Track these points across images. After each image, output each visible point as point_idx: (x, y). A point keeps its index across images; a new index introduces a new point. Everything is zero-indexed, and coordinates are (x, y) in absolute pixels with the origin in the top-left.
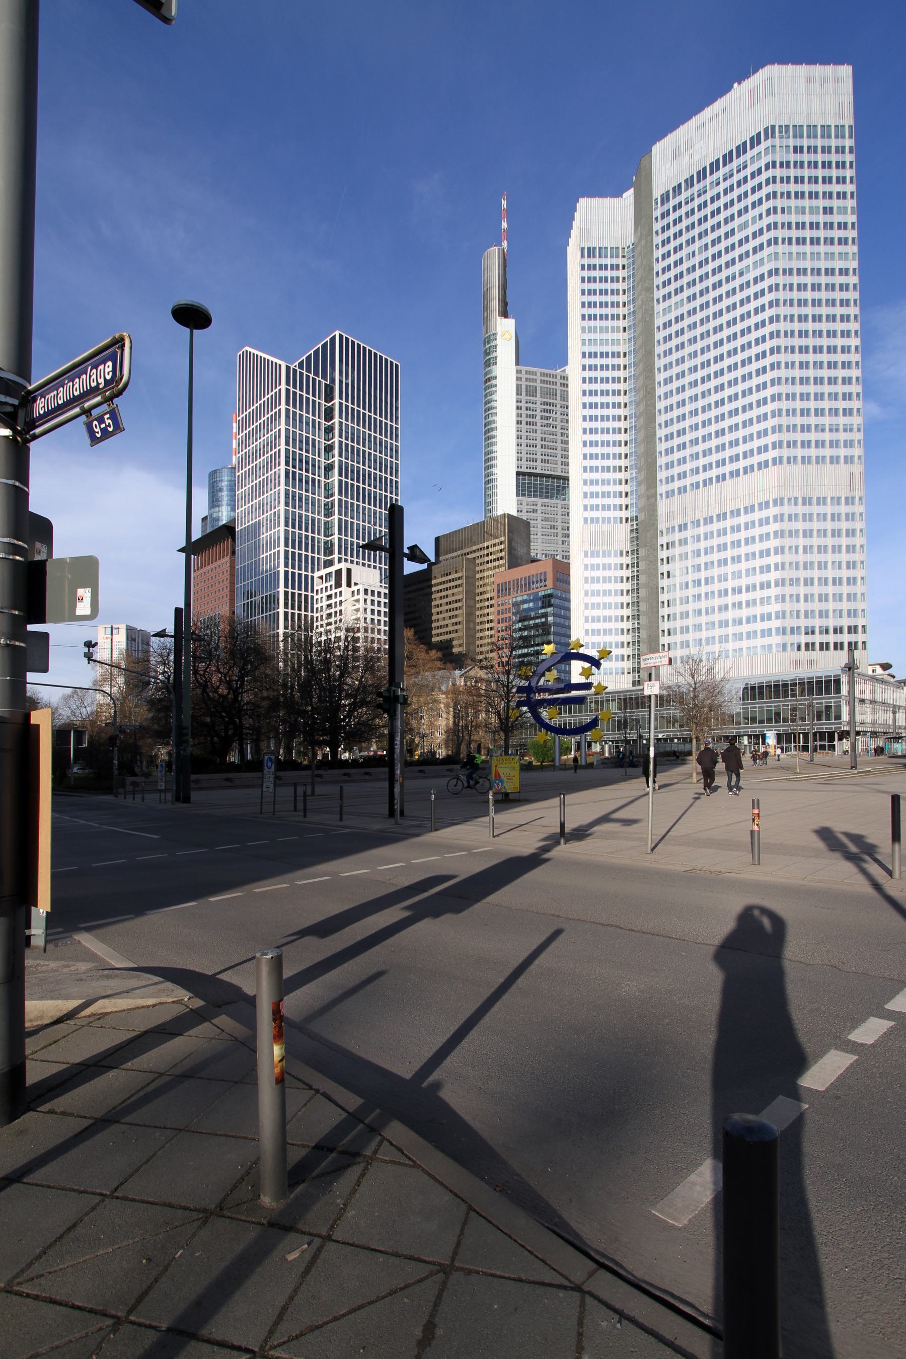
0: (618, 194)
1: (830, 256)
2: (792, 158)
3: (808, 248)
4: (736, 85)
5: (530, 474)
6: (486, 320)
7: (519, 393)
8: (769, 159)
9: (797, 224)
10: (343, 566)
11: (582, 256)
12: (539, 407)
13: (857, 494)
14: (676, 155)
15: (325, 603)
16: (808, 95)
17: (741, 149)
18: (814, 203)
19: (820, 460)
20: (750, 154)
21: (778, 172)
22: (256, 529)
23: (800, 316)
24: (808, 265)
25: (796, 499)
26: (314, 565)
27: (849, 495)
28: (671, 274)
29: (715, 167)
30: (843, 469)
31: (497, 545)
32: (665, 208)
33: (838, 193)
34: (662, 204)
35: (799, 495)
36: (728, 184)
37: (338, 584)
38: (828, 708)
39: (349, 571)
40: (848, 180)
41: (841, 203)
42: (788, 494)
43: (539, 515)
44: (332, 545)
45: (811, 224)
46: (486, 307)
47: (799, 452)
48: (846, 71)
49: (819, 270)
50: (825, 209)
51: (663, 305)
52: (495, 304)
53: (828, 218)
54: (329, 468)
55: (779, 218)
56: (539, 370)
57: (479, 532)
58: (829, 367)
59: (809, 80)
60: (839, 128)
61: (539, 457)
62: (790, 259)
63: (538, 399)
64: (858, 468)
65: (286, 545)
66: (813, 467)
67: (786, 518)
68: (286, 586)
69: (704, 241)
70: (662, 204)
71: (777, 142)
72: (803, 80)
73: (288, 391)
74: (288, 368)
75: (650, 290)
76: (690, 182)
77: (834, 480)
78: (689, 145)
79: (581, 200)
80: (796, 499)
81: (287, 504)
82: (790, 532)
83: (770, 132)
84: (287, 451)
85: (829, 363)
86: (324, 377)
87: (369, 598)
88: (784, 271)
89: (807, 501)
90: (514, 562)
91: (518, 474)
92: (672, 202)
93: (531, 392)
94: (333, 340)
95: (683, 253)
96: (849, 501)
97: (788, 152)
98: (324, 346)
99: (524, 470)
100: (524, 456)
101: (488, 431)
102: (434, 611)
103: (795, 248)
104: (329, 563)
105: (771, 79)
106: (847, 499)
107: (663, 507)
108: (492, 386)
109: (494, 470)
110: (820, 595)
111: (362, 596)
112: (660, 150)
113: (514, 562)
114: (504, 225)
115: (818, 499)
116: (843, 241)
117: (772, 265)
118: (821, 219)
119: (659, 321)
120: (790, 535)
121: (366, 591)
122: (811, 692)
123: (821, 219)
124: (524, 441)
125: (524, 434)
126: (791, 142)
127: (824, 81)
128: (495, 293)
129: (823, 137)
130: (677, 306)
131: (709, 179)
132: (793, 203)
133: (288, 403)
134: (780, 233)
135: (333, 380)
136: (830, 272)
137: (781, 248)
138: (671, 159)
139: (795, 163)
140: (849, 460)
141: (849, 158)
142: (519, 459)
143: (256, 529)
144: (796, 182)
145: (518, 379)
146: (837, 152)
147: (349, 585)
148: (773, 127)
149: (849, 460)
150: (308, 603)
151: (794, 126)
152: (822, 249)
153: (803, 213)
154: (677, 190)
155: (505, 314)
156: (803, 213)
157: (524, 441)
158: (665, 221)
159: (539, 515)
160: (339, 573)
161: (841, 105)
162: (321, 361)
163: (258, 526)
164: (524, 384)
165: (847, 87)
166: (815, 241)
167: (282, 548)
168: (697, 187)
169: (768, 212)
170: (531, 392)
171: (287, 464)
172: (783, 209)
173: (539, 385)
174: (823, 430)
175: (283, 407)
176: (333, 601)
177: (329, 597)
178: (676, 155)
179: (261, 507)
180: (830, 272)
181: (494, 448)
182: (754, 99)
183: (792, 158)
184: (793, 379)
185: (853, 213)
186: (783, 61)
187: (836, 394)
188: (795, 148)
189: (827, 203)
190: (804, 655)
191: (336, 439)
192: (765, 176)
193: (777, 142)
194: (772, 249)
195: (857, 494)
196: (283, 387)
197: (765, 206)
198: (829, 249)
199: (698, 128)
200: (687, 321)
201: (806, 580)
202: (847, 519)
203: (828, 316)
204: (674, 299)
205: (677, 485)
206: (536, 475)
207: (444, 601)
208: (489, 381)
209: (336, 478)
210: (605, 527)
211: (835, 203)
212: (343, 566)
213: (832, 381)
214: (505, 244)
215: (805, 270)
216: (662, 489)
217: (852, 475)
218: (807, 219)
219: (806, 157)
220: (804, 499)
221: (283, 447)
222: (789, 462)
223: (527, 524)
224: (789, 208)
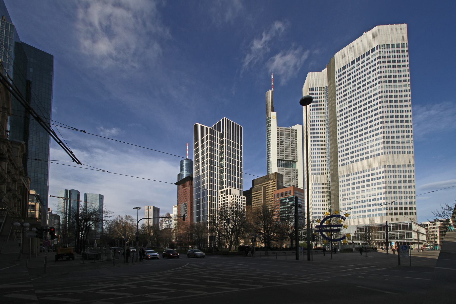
0: (321, 70)
1: (401, 86)
2: (386, 55)
3: (393, 84)
4: (364, 33)
5: (282, 160)
6: (267, 113)
7: (278, 135)
8: (378, 55)
9: (389, 76)
10: (228, 188)
11: (310, 91)
12: (284, 139)
13: (412, 164)
14: (343, 56)
15: (222, 200)
16: (394, 34)
17: (368, 53)
18: (395, 69)
19: (398, 153)
20: (371, 54)
21: (382, 60)
22: (200, 177)
23: (390, 106)
24: (393, 89)
25: (390, 166)
26: (217, 188)
27: (409, 164)
28: (342, 95)
29: (358, 59)
30: (407, 155)
31: (273, 183)
32: (340, 74)
33: (403, 65)
34: (339, 72)
35: (391, 164)
36: (363, 64)
37: (227, 194)
38: (407, 234)
39: (230, 190)
40: (406, 61)
41: (404, 68)
42: (387, 164)
43: (285, 173)
44: (223, 182)
45: (394, 76)
46: (267, 109)
47: (391, 150)
48: (404, 26)
49: (397, 91)
50: (398, 71)
51: (339, 105)
52: (270, 108)
53: (400, 74)
54: (222, 159)
55: (382, 75)
56: (284, 128)
57: (267, 178)
58: (401, 122)
59: (391, 29)
60: (403, 45)
61: (284, 155)
62: (386, 87)
63: (284, 137)
64: (412, 155)
65: (210, 182)
66: (396, 155)
67: (387, 172)
68: (210, 194)
69: (354, 83)
70: (339, 72)
71: (381, 50)
72: (390, 30)
73: (210, 136)
74: (210, 129)
75: (335, 100)
76: (349, 65)
77: (403, 159)
78: (349, 53)
79: (309, 73)
80: (390, 166)
81: (210, 170)
82: (388, 176)
83: (378, 47)
84: (210, 154)
85: (401, 121)
86: (220, 131)
87: (237, 198)
88: (385, 91)
89: (394, 166)
90: (278, 188)
91: (278, 160)
92: (342, 72)
93: (282, 134)
94: (223, 120)
95: (347, 88)
96: (409, 166)
97: (385, 53)
98: (220, 122)
99: (280, 159)
100: (280, 154)
101: (268, 147)
102: (253, 202)
103: (388, 84)
104: (222, 188)
105: (378, 30)
106: (408, 165)
107: (340, 169)
108: (269, 133)
109: (270, 159)
110: (399, 197)
111: (234, 198)
112: (337, 55)
113: (278, 188)
114: (272, 84)
115: (398, 165)
116: (405, 81)
117: (380, 90)
118: (397, 74)
119: (338, 110)
120: (388, 177)
121: (236, 196)
122: (397, 229)
123: (397, 74)
124: (280, 150)
125: (280, 147)
126: (386, 50)
127: (397, 29)
128: (270, 104)
129: (397, 47)
130: (345, 104)
131: (356, 64)
132: (387, 69)
133: (210, 139)
134: (383, 79)
135: (223, 132)
136: (400, 91)
137: (383, 84)
138: (341, 59)
139: (388, 56)
140: (409, 152)
141: (406, 54)
142: (278, 155)
143: (200, 177)
144: (388, 62)
145: (278, 131)
146: (402, 52)
147: (230, 194)
148: (380, 45)
149: (409, 152)
150: (217, 200)
151: (387, 45)
152: (398, 84)
153: (391, 72)
154: (344, 68)
155: (273, 111)
156: (391, 72)
157: (280, 150)
158: (340, 78)
159: (285, 173)
160: (227, 191)
161: (403, 37)
162: (219, 127)
163: (201, 176)
164: (279, 132)
165: (405, 31)
166: (395, 81)
167: (209, 183)
168: (351, 66)
169: (378, 73)
170: (282, 134)
171: (210, 157)
172: (384, 72)
173: (284, 132)
174: (399, 143)
175: (209, 140)
176: (225, 199)
177: (224, 198)
178: (343, 56)
179: (202, 171)
180: (400, 91)
181: (270, 152)
182: (372, 36)
183: (386, 55)
184: (388, 126)
185: (408, 72)
186: (382, 24)
187: (404, 131)
188: (387, 52)
189: (399, 69)
190: (394, 217)
191: (224, 150)
192: (377, 61)
193: (381, 50)
194: (380, 85)
195: (412, 164)
196: (209, 134)
197: (377, 71)
198: (400, 84)
199: (352, 48)
200: (348, 109)
201: (394, 192)
202: (408, 172)
203: (400, 106)
204: (343, 103)
205: (345, 162)
206: (284, 160)
207: (256, 199)
208: (268, 132)
209: (224, 162)
210: (318, 176)
211: (402, 69)
212: (228, 188)
213: (402, 127)
214: (273, 89)
215: (392, 91)
216: (340, 163)
217: (410, 157)
218: (392, 74)
219: (391, 54)
220: (393, 166)
221: (209, 153)
222: (387, 154)
223: (282, 176)
224: (386, 71)
